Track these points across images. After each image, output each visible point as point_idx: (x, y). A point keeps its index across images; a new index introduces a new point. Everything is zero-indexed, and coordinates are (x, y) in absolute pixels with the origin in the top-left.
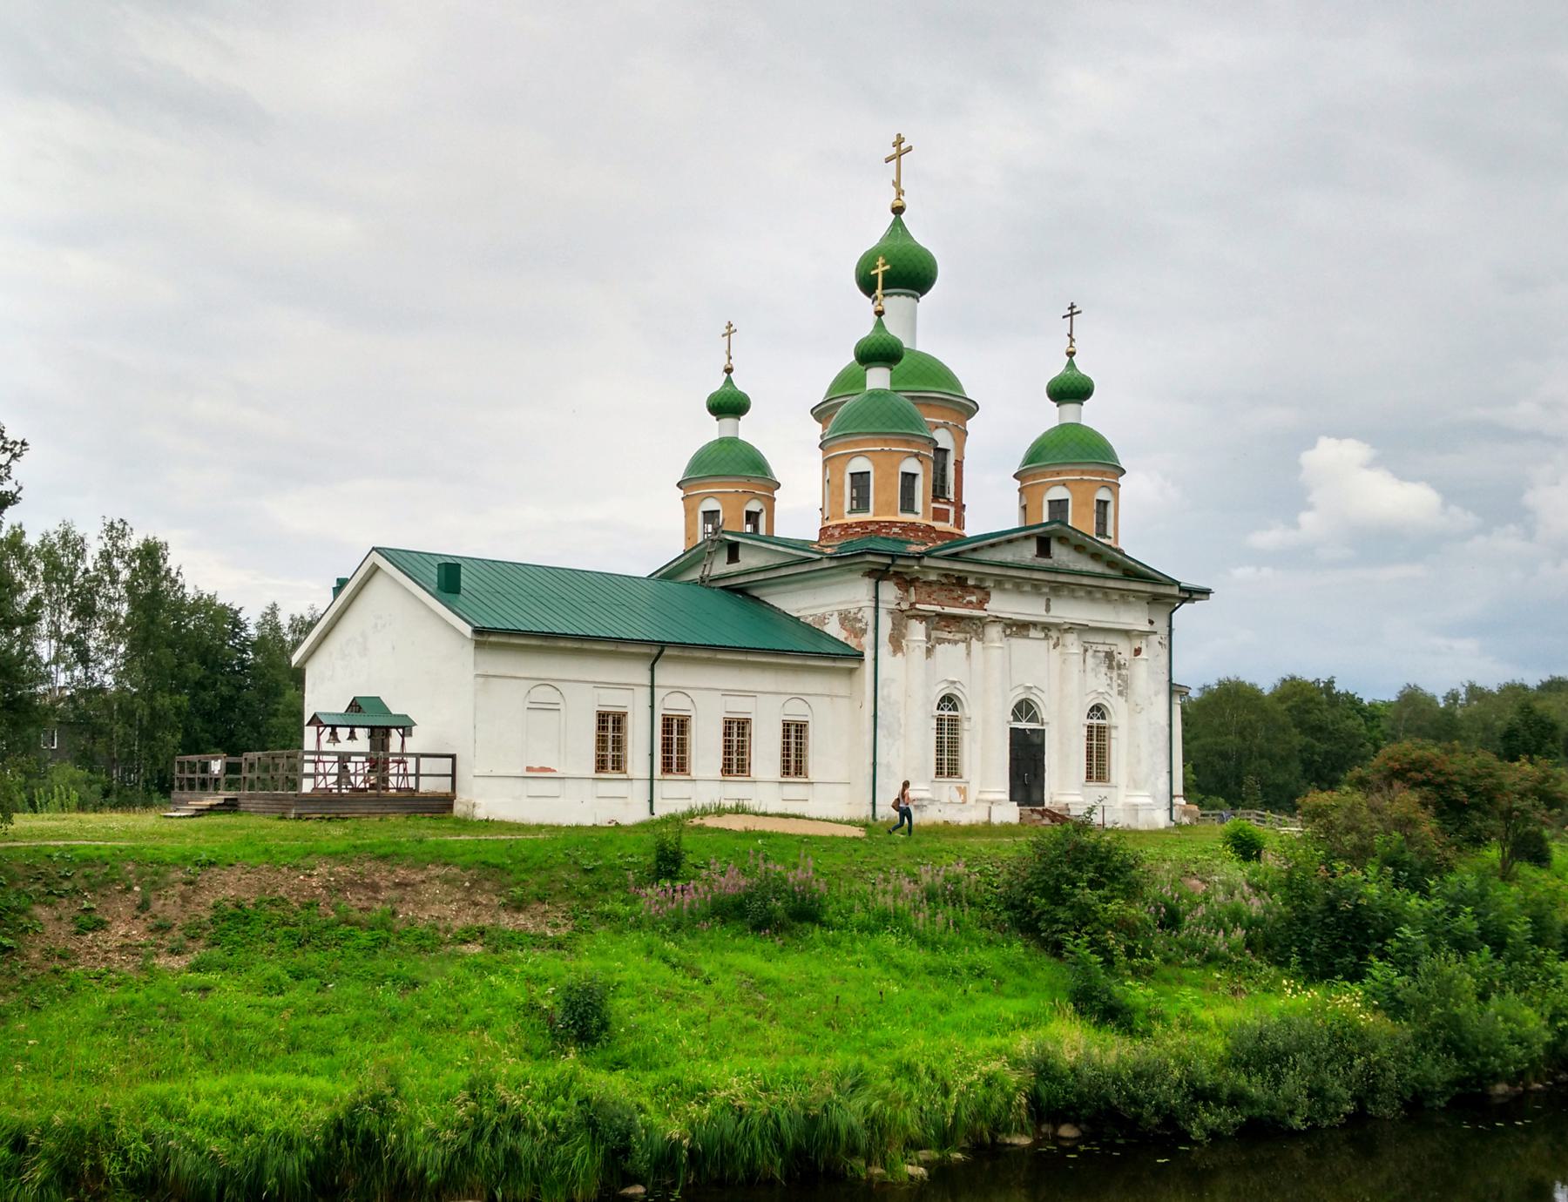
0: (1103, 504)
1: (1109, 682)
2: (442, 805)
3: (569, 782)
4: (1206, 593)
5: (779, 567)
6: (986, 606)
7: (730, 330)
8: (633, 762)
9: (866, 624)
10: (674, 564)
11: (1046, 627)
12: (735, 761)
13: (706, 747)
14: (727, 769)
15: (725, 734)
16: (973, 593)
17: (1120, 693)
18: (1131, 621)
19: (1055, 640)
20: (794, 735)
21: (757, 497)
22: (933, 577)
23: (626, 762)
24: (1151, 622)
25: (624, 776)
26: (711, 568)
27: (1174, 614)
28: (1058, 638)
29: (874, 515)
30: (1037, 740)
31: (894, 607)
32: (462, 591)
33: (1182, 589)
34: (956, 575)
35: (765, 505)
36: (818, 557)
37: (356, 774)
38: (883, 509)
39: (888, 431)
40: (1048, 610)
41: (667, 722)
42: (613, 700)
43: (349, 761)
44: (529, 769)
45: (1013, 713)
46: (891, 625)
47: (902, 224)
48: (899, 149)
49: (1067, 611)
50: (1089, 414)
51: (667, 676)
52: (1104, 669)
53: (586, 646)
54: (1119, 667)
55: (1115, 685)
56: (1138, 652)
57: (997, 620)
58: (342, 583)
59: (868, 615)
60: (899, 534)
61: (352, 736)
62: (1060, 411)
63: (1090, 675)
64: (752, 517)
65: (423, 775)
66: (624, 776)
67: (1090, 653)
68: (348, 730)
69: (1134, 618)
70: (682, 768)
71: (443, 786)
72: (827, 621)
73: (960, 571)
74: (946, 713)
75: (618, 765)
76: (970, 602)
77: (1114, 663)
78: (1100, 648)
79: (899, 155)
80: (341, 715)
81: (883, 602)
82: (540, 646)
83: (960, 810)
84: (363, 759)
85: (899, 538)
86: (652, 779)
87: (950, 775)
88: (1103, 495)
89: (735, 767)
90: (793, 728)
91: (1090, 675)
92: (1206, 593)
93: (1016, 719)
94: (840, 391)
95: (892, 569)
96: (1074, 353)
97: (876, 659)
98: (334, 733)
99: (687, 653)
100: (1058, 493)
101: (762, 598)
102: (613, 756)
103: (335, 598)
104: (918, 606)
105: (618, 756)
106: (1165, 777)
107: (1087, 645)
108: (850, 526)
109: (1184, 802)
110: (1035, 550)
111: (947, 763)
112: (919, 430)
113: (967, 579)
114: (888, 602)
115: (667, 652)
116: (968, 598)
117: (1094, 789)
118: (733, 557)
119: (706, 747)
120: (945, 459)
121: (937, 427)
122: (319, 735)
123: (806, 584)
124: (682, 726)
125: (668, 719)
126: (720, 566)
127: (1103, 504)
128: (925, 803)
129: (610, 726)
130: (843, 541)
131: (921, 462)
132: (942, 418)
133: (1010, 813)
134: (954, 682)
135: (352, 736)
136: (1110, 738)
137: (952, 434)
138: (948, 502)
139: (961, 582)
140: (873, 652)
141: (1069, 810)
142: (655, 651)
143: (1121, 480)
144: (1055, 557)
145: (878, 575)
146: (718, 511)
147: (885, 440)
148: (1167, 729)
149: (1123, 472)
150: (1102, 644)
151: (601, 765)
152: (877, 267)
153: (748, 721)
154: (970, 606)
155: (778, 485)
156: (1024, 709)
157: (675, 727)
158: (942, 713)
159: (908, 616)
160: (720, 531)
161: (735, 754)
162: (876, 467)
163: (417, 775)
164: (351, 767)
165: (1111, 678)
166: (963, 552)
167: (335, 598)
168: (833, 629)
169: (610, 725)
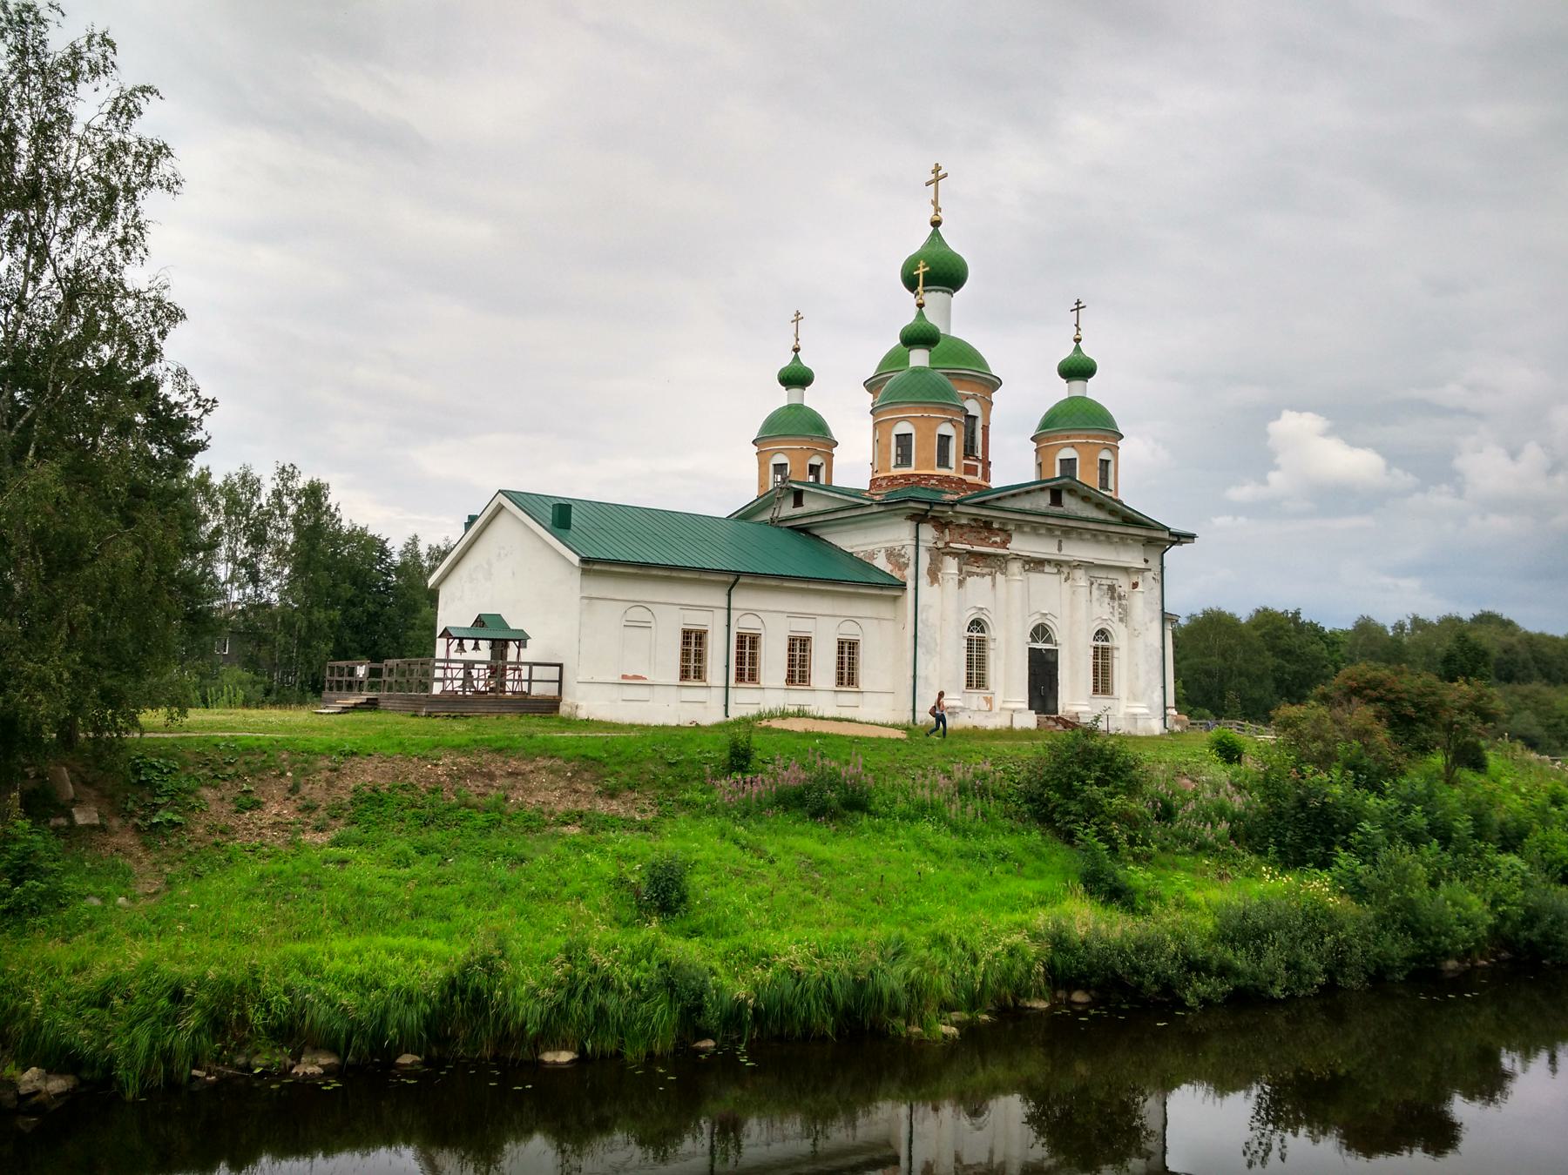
0: (1105, 463)
2: (550, 706)
3: (656, 688)
4: (1191, 537)
7: (798, 317)
9: (909, 559)
11: (1059, 564)
12: (798, 672)
14: (790, 679)
15: (789, 650)
17: (1121, 620)
19: (1066, 574)
20: (848, 652)
22: (964, 521)
23: (706, 672)
24: (1146, 561)
25: (856, 690)
31: (931, 545)
32: (572, 527)
33: (1171, 534)
37: (478, 679)
38: (922, 464)
40: (1060, 549)
41: (741, 639)
42: (696, 620)
44: (624, 677)
45: (1031, 635)
47: (939, 234)
48: (937, 176)
50: (1093, 389)
51: (743, 600)
52: (1107, 600)
53: (674, 574)
54: (1120, 598)
55: (1116, 613)
56: (1135, 585)
57: (1018, 557)
59: (910, 552)
61: (476, 647)
63: (1095, 604)
69: (1132, 557)
70: (753, 677)
71: (552, 690)
73: (987, 516)
75: (699, 674)
76: (995, 542)
77: (1116, 595)
78: (1104, 582)
81: (923, 541)
84: (485, 666)
86: (727, 687)
87: (978, 687)
88: (1105, 455)
89: (797, 678)
90: (846, 645)
91: (1095, 604)
93: (1034, 640)
95: (929, 514)
96: (1080, 340)
97: (916, 588)
98: (461, 645)
99: (758, 581)
104: (951, 545)
108: (895, 478)
109: (1176, 713)
111: (976, 678)
118: (798, 502)
122: (448, 646)
123: (858, 525)
126: (787, 509)
127: (1105, 463)
128: (957, 710)
129: (693, 642)
130: (889, 490)
131: (954, 426)
133: (1028, 720)
134: (982, 609)
135: (476, 647)
138: (977, 459)
140: (914, 582)
142: (732, 579)
143: (1120, 443)
145: (919, 518)
147: (925, 408)
148: (1161, 651)
150: (1106, 579)
151: (685, 675)
153: (809, 639)
156: (1041, 632)
157: (748, 643)
162: (917, 429)
163: (530, 681)
165: (1113, 607)
166: (989, 500)
168: (881, 562)
169: (693, 640)
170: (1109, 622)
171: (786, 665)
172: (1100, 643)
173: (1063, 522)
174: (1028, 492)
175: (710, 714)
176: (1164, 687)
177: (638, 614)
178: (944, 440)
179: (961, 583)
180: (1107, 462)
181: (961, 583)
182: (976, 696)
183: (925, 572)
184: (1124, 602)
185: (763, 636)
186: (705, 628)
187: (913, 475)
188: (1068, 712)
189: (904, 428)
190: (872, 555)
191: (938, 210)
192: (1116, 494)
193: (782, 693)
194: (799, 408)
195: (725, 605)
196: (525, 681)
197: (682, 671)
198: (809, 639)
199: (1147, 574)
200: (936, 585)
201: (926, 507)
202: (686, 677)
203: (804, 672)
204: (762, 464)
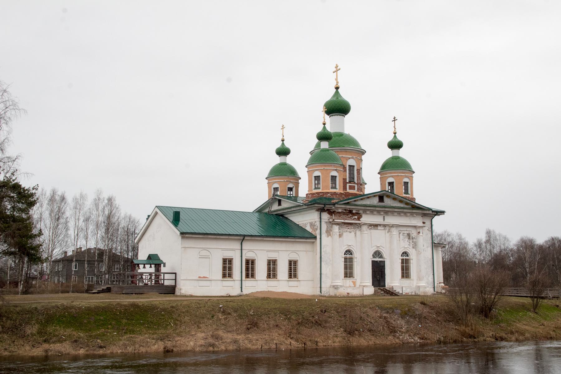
0: (406, 184)
1: (409, 244)
2: (172, 290)
3: (213, 282)
4: (443, 212)
6: (361, 219)
7: (283, 127)
8: (235, 275)
9: (317, 227)
10: (262, 206)
11: (385, 226)
13: (261, 269)
14: (269, 276)
15: (268, 265)
16: (355, 215)
17: (413, 247)
18: (416, 223)
19: (388, 230)
21: (292, 182)
22: (340, 211)
24: (424, 223)
26: (271, 208)
27: (433, 220)
28: (389, 229)
29: (322, 190)
30: (382, 265)
31: (327, 221)
33: (433, 211)
35: (295, 185)
36: (302, 204)
37: (145, 279)
38: (325, 188)
39: (325, 162)
40: (384, 220)
41: (247, 262)
42: (228, 255)
43: (143, 275)
44: (200, 277)
45: (373, 255)
46: (326, 227)
48: (337, 69)
49: (391, 220)
50: (402, 153)
51: (247, 246)
52: (407, 239)
54: (413, 238)
55: (411, 245)
56: (419, 233)
57: (365, 224)
58: (149, 216)
59: (318, 224)
60: (330, 196)
61: (144, 267)
62: (392, 152)
63: (401, 241)
65: (165, 280)
66: (232, 279)
67: (401, 234)
68: (143, 265)
69: (417, 221)
70: (253, 276)
71: (172, 283)
72: (306, 226)
73: (350, 208)
75: (230, 276)
76: (355, 218)
77: (411, 237)
78: (405, 232)
80: (146, 260)
81: (323, 219)
82: (203, 237)
83: (353, 289)
84: (148, 274)
85: (331, 198)
87: (350, 277)
88: (406, 180)
89: (272, 276)
91: (401, 241)
92: (443, 212)
94: (317, 148)
97: (321, 238)
99: (253, 238)
100: (391, 180)
101: (288, 218)
102: (228, 273)
103: (147, 221)
104: (335, 220)
105: (230, 273)
106: (432, 276)
107: (400, 231)
108: (314, 194)
109: (444, 285)
110: (378, 200)
111: (349, 273)
112: (336, 162)
113: (352, 211)
114: (325, 219)
115: (246, 238)
116: (354, 217)
117: (404, 281)
118: (280, 204)
119: (261, 269)
120: (353, 168)
121: (349, 159)
123: (300, 213)
124: (253, 262)
125: (248, 260)
126: (275, 207)
127: (406, 184)
128: (339, 287)
129: (227, 265)
130: (312, 199)
131: (338, 172)
132: (351, 155)
134: (350, 246)
135: (144, 267)
136: (410, 263)
137: (355, 161)
138: (355, 183)
140: (320, 236)
141: (393, 288)
142: (242, 238)
143: (414, 175)
144: (386, 202)
145: (322, 210)
146: (278, 188)
148: (432, 260)
149: (414, 172)
150: (406, 231)
151: (224, 276)
154: (355, 219)
155: (300, 178)
157: (250, 263)
158: (346, 256)
159: (332, 224)
160: (275, 195)
161: (272, 272)
162: (322, 174)
163: (164, 279)
164: (144, 277)
165: (410, 243)
166: (351, 202)
167: (147, 221)
168: (308, 228)
170: (408, 249)
171: (267, 271)
172: (404, 257)
173: (383, 209)
174: (368, 198)
175: (235, 292)
176: (434, 275)
177: (204, 253)
178: (334, 178)
179: (340, 236)
181: (340, 236)
182: (348, 281)
183: (325, 232)
184: (414, 240)
185: (256, 260)
186: (232, 257)
187: (321, 193)
188: (390, 286)
190: (306, 225)
191: (395, 129)
192: (412, 194)
193: (265, 282)
194: (284, 164)
195: (240, 248)
196: (162, 279)
197: (223, 275)
199: (424, 228)
200: (330, 237)
201: (323, 206)
202: (225, 277)
203: (274, 273)
204: (269, 187)
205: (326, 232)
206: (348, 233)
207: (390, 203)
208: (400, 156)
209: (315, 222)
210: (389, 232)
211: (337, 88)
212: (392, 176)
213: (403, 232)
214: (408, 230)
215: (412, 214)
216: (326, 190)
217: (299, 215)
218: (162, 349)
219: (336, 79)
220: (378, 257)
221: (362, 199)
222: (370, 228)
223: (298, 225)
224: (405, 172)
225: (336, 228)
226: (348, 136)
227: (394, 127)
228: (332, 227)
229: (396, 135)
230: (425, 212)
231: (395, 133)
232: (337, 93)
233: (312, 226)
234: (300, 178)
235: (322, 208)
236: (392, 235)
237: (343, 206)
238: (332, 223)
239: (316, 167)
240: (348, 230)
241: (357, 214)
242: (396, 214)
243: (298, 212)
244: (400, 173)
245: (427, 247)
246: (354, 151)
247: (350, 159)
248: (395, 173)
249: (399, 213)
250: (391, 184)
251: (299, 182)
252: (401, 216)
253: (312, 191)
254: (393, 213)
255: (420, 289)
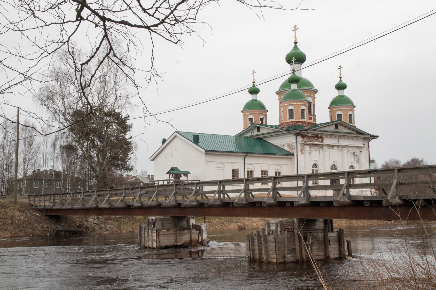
0: (350, 115)
4: (377, 137)
5: (271, 133)
6: (323, 142)
7: (295, 29)
9: (295, 147)
11: (338, 146)
15: (262, 175)
16: (320, 139)
17: (357, 162)
22: (310, 135)
24: (364, 144)
33: (371, 136)
34: (316, 134)
36: (282, 130)
39: (297, 99)
40: (338, 142)
41: (248, 172)
42: (236, 167)
45: (331, 168)
49: (343, 142)
50: (346, 93)
52: (353, 156)
54: (356, 156)
55: (355, 160)
56: (361, 151)
57: (326, 145)
59: (295, 145)
64: (262, 120)
67: (349, 152)
69: (359, 143)
73: (317, 133)
74: (314, 168)
76: (319, 141)
77: (355, 155)
79: (295, 30)
81: (299, 141)
88: (350, 113)
92: (377, 137)
93: (332, 169)
95: (300, 133)
97: (297, 155)
98: (172, 176)
99: (253, 155)
104: (307, 142)
108: (289, 123)
113: (318, 135)
116: (319, 140)
122: (170, 176)
126: (255, 133)
127: (350, 115)
132: (309, 94)
134: (316, 161)
138: (312, 115)
139: (317, 136)
142: (245, 155)
143: (355, 109)
144: (339, 129)
145: (297, 135)
149: (355, 107)
150: (352, 150)
152: (292, 60)
153: (267, 171)
155: (268, 111)
157: (250, 173)
162: (295, 108)
165: (355, 159)
166: (317, 129)
168: (286, 148)
170: (354, 163)
174: (328, 126)
177: (220, 166)
179: (310, 153)
180: (351, 115)
181: (310, 153)
183: (299, 150)
184: (358, 157)
189: (291, 107)
191: (341, 74)
192: (354, 124)
195: (243, 162)
198: (267, 171)
200: (303, 154)
201: (299, 131)
205: (300, 151)
206: (314, 152)
207: (342, 129)
208: (345, 95)
209: (293, 143)
210: (341, 151)
211: (296, 43)
212: (340, 110)
213: (350, 151)
214: (353, 149)
215: (357, 138)
216: (298, 120)
217: (277, 138)
218: (237, 227)
219: (295, 37)
220: (334, 168)
221: (324, 127)
222: (329, 148)
223: (276, 146)
224: (350, 107)
225: (307, 148)
226: (305, 79)
227: (340, 73)
228: (304, 147)
229: (341, 79)
230: (366, 136)
231: (341, 78)
232: (296, 47)
233: (289, 146)
234: (268, 111)
235: (298, 133)
236: (344, 153)
237: (313, 132)
238: (304, 144)
239: (290, 103)
240: (315, 149)
241: (321, 137)
242: (346, 138)
243: (276, 136)
244: (346, 107)
245: (366, 162)
246: (311, 91)
247: (308, 97)
248: (342, 107)
249: (348, 137)
250: (340, 116)
251: (267, 114)
252: (349, 139)
253: (287, 120)
254: (344, 137)
255: (362, 193)
